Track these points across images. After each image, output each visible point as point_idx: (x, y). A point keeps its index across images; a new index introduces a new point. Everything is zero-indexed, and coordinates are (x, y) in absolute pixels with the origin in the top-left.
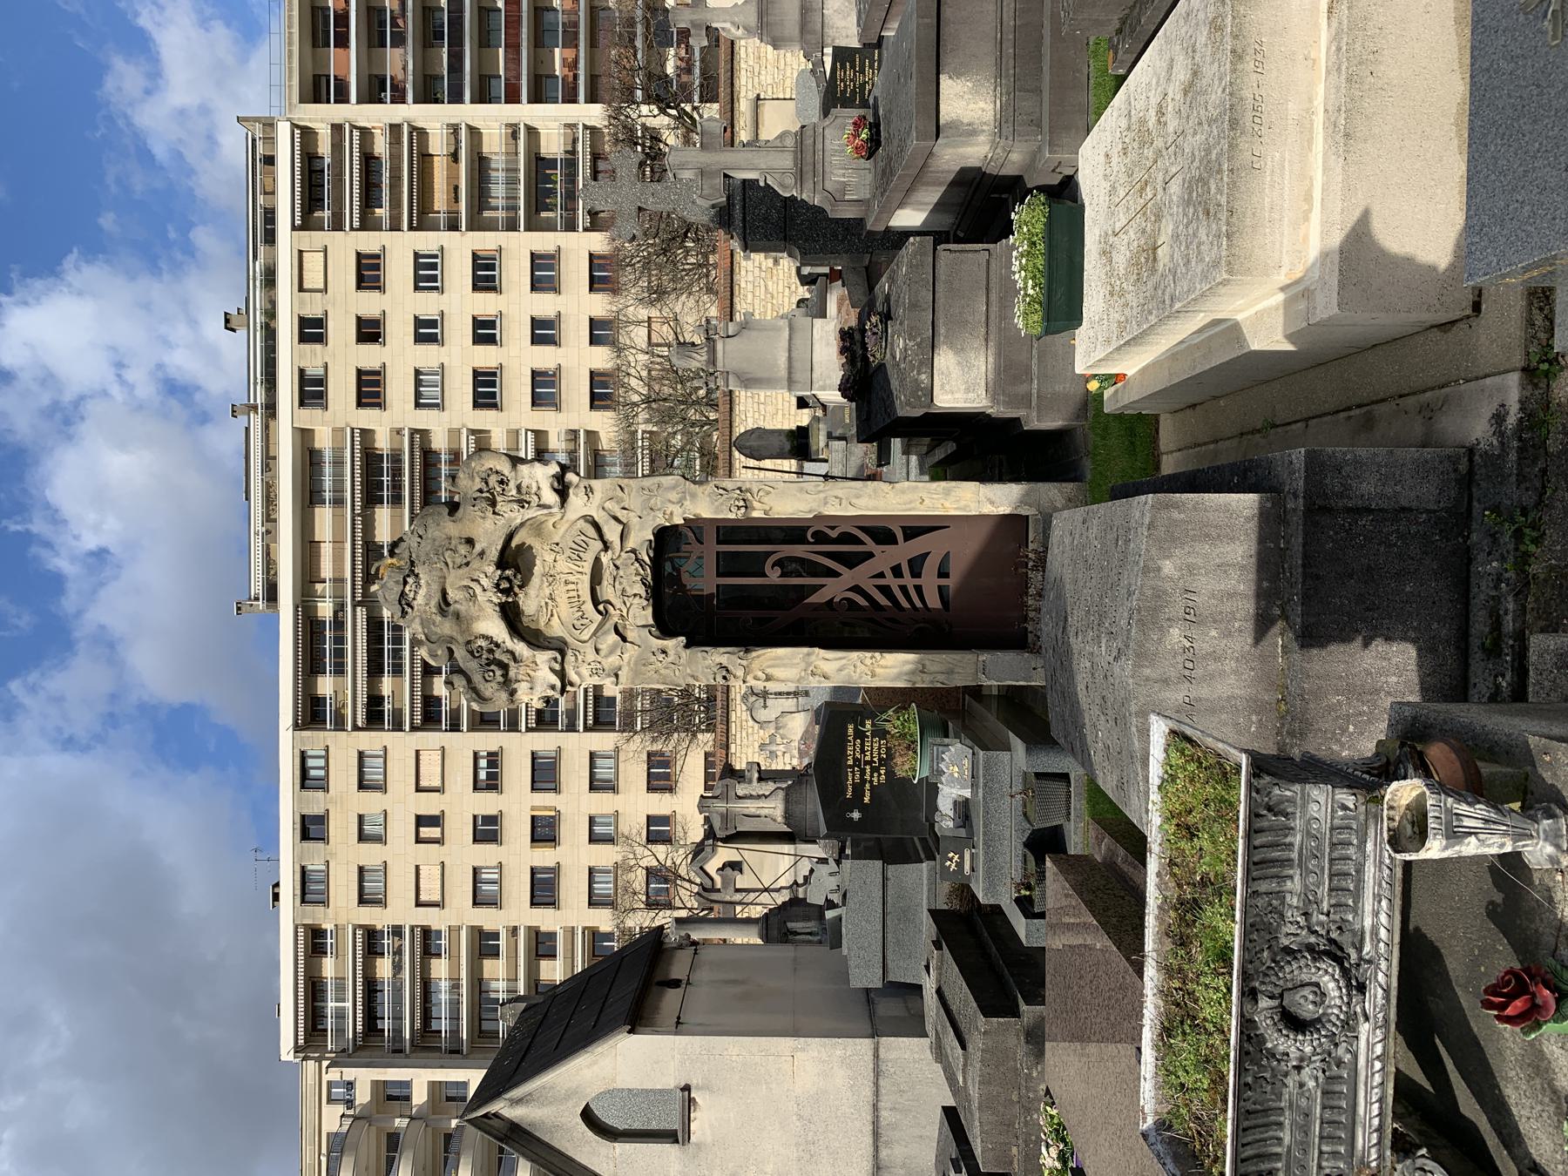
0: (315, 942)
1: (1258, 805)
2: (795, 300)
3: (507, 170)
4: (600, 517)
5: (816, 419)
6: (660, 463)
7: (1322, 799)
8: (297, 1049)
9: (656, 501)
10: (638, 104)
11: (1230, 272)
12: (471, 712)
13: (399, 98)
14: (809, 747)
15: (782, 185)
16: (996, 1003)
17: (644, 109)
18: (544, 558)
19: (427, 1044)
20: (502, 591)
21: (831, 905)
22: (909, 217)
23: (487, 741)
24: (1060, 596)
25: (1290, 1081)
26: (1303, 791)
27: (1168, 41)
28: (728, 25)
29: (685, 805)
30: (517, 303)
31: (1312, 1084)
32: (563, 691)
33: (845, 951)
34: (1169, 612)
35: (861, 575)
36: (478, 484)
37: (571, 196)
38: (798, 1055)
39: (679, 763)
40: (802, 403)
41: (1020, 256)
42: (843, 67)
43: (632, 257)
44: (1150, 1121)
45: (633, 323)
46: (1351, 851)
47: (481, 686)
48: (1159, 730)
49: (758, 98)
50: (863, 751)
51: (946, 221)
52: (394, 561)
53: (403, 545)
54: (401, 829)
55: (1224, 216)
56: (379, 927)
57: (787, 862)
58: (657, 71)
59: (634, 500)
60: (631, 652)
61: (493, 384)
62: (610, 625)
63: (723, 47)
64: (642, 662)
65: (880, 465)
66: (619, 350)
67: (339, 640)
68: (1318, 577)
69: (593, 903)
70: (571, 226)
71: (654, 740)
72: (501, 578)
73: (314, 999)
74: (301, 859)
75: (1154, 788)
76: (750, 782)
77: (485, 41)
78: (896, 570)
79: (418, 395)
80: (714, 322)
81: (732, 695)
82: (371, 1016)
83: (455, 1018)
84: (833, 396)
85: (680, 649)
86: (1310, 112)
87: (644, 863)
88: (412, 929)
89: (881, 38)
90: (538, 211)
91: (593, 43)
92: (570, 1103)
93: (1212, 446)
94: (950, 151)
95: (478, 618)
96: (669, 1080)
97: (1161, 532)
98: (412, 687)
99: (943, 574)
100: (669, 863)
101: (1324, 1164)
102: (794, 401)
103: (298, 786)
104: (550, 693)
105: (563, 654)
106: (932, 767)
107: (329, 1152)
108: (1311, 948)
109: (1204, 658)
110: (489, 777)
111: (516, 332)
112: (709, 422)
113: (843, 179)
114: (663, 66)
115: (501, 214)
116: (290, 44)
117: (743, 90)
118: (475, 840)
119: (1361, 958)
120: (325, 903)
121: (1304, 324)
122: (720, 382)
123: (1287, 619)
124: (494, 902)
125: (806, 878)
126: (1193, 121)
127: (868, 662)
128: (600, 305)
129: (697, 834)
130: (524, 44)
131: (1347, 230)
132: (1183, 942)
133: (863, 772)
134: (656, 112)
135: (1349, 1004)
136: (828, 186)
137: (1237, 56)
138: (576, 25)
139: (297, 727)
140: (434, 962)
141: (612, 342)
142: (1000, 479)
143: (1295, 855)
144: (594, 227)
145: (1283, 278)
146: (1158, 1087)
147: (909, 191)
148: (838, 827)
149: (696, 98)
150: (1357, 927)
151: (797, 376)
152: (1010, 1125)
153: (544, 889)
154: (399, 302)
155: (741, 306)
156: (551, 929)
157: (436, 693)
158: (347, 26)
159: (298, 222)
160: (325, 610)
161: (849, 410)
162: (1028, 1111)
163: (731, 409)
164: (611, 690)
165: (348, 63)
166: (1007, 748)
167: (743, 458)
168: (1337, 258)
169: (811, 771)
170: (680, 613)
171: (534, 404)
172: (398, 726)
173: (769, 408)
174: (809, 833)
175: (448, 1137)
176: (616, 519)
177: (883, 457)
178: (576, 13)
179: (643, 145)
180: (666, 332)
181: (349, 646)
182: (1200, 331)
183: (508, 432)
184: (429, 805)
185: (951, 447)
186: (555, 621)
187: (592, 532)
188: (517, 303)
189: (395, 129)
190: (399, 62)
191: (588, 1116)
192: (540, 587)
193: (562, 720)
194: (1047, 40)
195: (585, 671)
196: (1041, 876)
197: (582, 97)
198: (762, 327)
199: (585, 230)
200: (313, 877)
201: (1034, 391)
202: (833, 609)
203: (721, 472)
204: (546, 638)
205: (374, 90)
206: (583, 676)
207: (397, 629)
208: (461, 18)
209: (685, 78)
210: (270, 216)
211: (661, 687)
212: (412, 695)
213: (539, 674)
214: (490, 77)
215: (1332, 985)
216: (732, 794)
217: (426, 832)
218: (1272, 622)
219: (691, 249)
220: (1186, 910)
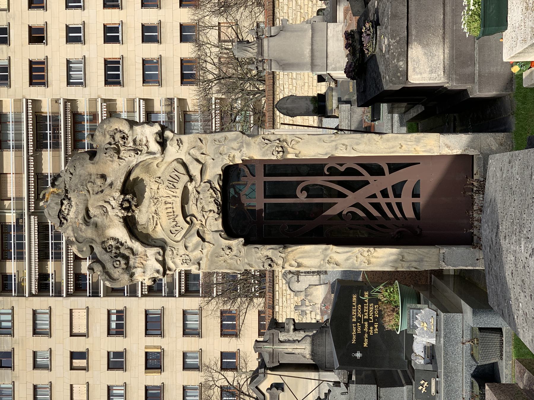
2: (316, 9)
4: (187, 159)
5: (330, 89)
9: (224, 149)
12: (106, 288)
14: (327, 308)
18: (151, 187)
20: (124, 209)
23: (116, 303)
24: (494, 212)
29: (246, 344)
32: (164, 274)
35: (360, 196)
36: (108, 139)
39: (242, 318)
40: (321, 79)
45: (208, 27)
47: (112, 271)
50: (363, 312)
52: (55, 189)
53: (60, 179)
54: (61, 361)
57: (313, 384)
61: (117, 69)
62: (194, 230)
64: (215, 255)
65: (373, 120)
66: (200, 45)
67: (20, 237)
71: (225, 303)
72: (124, 200)
76: (288, 331)
78: (384, 194)
79: (69, 77)
80: (262, 25)
84: (340, 75)
85: (241, 246)
87: (219, 384)
95: (109, 227)
98: (67, 268)
99: (415, 195)
100: (235, 384)
102: (316, 77)
104: (156, 275)
106: (409, 323)
110: (118, 327)
118: (109, 368)
122: (266, 66)
125: (326, 395)
127: (366, 254)
129: (253, 365)
133: (363, 326)
142: (454, 131)
148: (346, 362)
151: (318, 61)
155: (280, 15)
157: (83, 271)
161: (352, 85)
163: (274, 83)
164: (194, 270)
166: (460, 311)
167: (282, 115)
169: (328, 324)
170: (240, 223)
171: (144, 82)
172: (58, 294)
174: (328, 365)
176: (198, 161)
177: (376, 115)
180: (230, 33)
181: (26, 242)
183: (128, 100)
184: (79, 345)
186: (159, 228)
187: (182, 169)
193: (165, 289)
198: (294, 29)
201: (477, 72)
202: (342, 219)
203: (267, 125)
204: (153, 239)
211: (229, 271)
212: (67, 273)
213: (149, 263)
216: (276, 339)
217: (77, 363)
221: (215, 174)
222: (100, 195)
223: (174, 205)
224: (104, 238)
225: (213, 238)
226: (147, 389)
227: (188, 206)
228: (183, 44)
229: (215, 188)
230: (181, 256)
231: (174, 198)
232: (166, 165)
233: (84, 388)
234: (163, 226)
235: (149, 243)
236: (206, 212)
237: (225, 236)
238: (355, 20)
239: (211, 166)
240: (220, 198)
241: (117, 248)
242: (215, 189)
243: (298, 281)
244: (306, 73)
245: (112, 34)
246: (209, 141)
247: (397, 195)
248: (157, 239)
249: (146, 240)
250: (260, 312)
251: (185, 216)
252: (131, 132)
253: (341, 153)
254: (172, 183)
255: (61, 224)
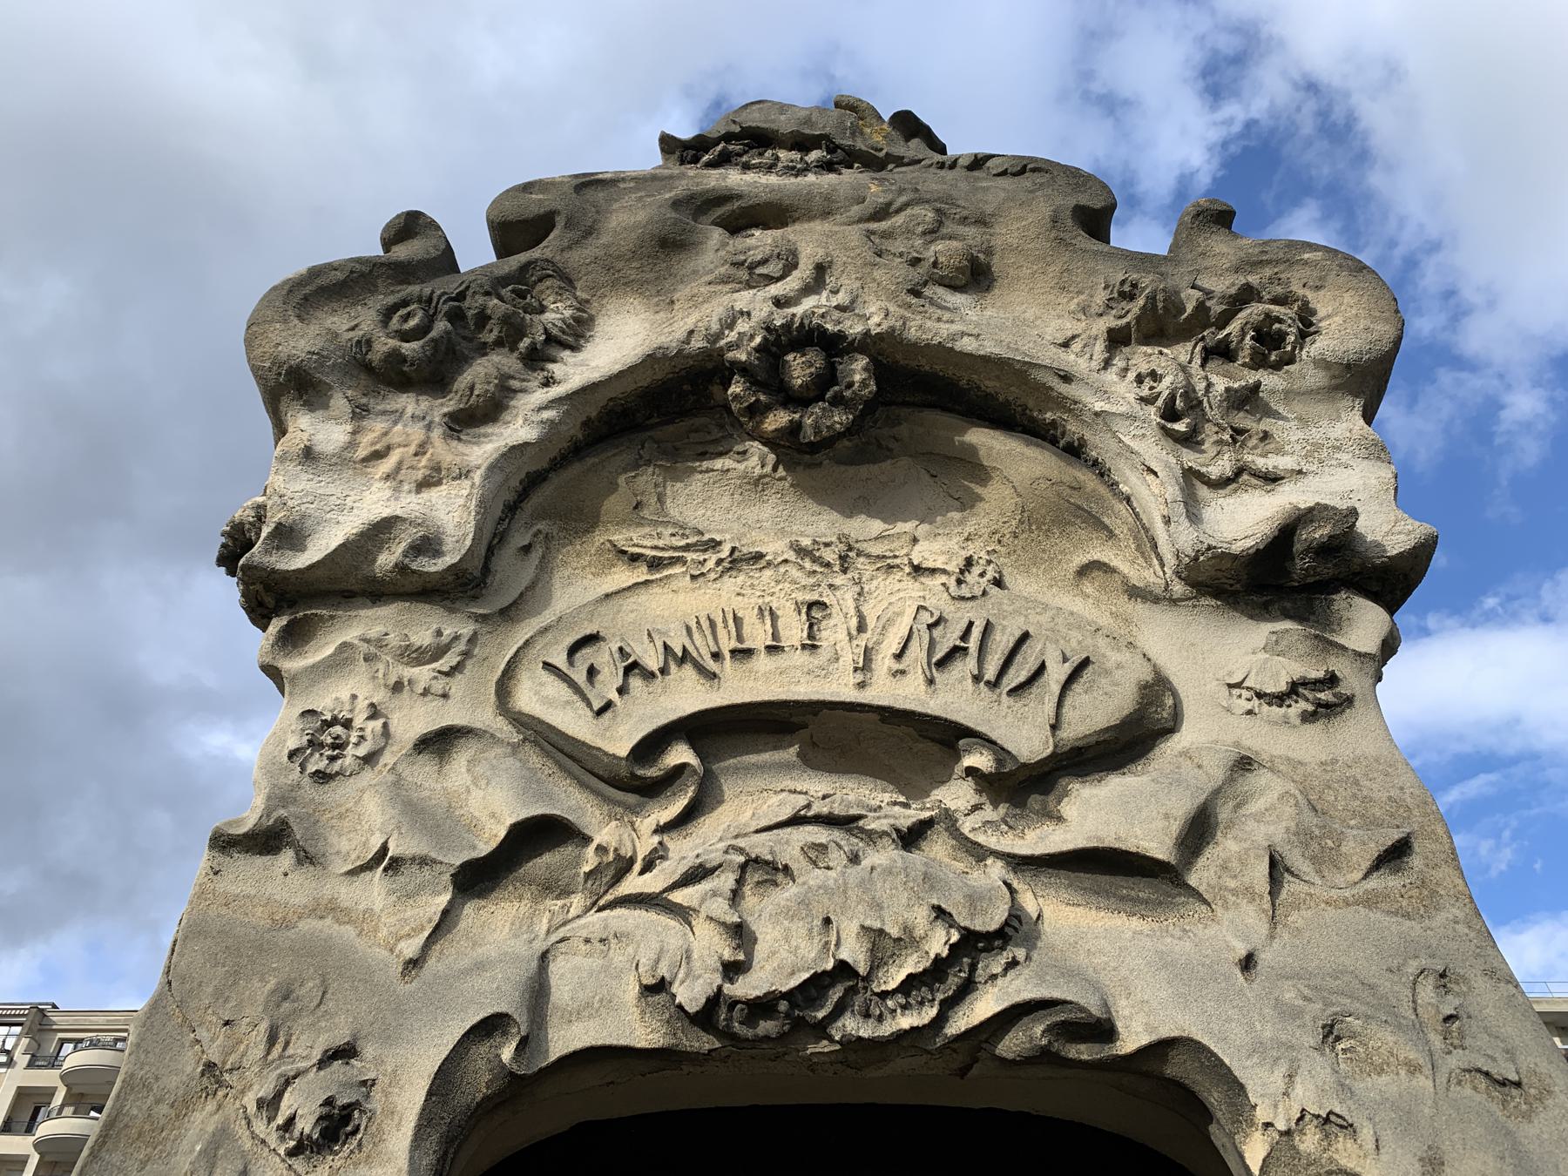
62: (570, 800)
176: (1199, 831)
187: (1094, 711)
221: (1105, 979)
223: (801, 658)
224: (593, 288)
225: (480, 966)
227: (786, 767)
229: (967, 989)
230: (374, 712)
231: (850, 655)
232: (1105, 620)
234: (631, 602)
235: (522, 516)
236: (735, 896)
237: (478, 1081)
239: (1182, 948)
240: (866, 1030)
242: (953, 982)
246: (1413, 928)
248: (545, 567)
249: (547, 498)
252: (1317, 379)
254: (973, 643)
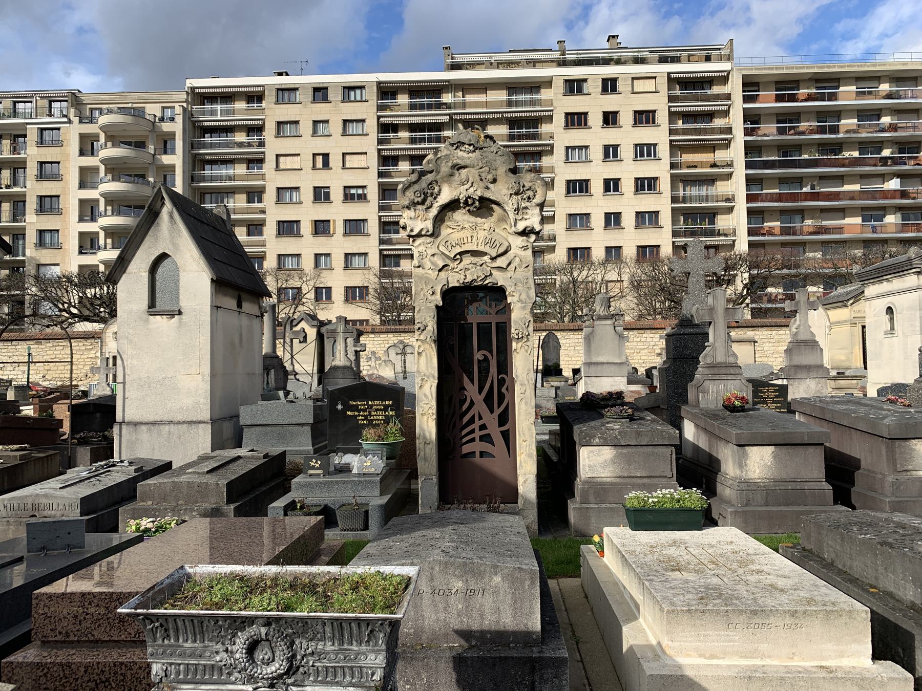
0: (255, 97)
1: (374, 625)
2: (636, 366)
3: (707, 196)
4: (510, 255)
5: (567, 380)
6: (541, 289)
7: (377, 661)
8: (193, 89)
9: (520, 287)
10: (749, 272)
11: (668, 612)
13: (747, 132)
15: (705, 357)
16: (235, 490)
17: (746, 275)
18: (486, 223)
19: (197, 162)
20: (466, 201)
21: (287, 393)
22: (689, 431)
23: (373, 193)
24: (475, 520)
25: (219, 646)
26: (382, 650)
27: (800, 575)
28: (798, 323)
30: (629, 204)
31: (218, 658)
32: (410, 236)
33: (260, 403)
34: (472, 581)
35: (480, 407)
36: (527, 185)
37: (693, 233)
38: (200, 377)
39: (363, 305)
40: (576, 372)
41: (669, 493)
42: (776, 391)
43: (659, 270)
44: (191, 571)
46: (348, 679)
47: (412, 190)
48: (410, 571)
49: (755, 342)
50: (377, 410)
51: (688, 452)
52: (483, 138)
54: (321, 145)
55: (701, 608)
56: (264, 133)
58: (770, 281)
59: (521, 274)
60: (433, 274)
61: (581, 191)
62: (448, 262)
63: (784, 320)
64: (427, 281)
65: (542, 417)
66: (603, 264)
67: (430, 107)
68: (494, 665)
69: (280, 256)
70: (675, 234)
71: (376, 290)
72: (474, 199)
73: (222, 97)
74: (303, 88)
75: (377, 568)
76: (355, 346)
77: (783, 181)
78: (483, 427)
79: (573, 148)
81: (403, 335)
82: (213, 130)
83: (212, 178)
84: (581, 389)
86: (763, 657)
88: (263, 153)
89: (794, 412)
90: (683, 214)
91: (784, 244)
92: (171, 246)
93: (563, 608)
94: (730, 454)
95: (450, 187)
96: (185, 303)
97: (517, 575)
99: (482, 454)
100: (304, 300)
101: (173, 667)
102: (577, 367)
103: (345, 85)
104: (409, 229)
105: (431, 236)
107: (134, 108)
108: (294, 656)
109: (446, 601)
110: (352, 195)
111: (612, 204)
112: (562, 317)
113: (712, 392)
114: (772, 285)
115: (681, 193)
116: (777, 68)
117: (760, 333)
118: (315, 188)
119: (288, 685)
120: (277, 103)
121: (639, 656)
122: (587, 323)
123: (469, 649)
124: (279, 200)
126: (755, 590)
127: (430, 411)
128: (629, 252)
129: (322, 316)
130: (782, 204)
131: (695, 679)
132: (292, 587)
133: (364, 410)
134: (745, 282)
135: (263, 678)
136: (707, 383)
137: (794, 614)
138: (794, 234)
139: (379, 83)
140: (244, 166)
141: (607, 260)
143: (346, 646)
144: (675, 247)
145: (665, 643)
146: (209, 574)
147: (705, 430)
149: (754, 306)
150: (306, 683)
151: (593, 368)
152: (165, 500)
153: (288, 228)
154: (627, 136)
156: (264, 233)
158: (788, 101)
159: (672, 76)
160: (447, 98)
162: (173, 510)
165: (767, 102)
168: (679, 673)
169: (362, 381)
170: (455, 301)
171: (570, 215)
172: (380, 141)
173: (572, 352)
175: (143, 176)
176: (509, 264)
177: (547, 419)
178: (801, 234)
179: (725, 275)
182: (632, 598)
185: (555, 458)
186: (450, 231)
187: (501, 250)
188: (629, 204)
189: (729, 130)
190: (768, 131)
191: (163, 256)
192: (469, 222)
194: (797, 509)
195: (421, 248)
196: (309, 514)
197: (752, 238)
199: (673, 243)
200: (292, 95)
204: (440, 226)
205: (752, 118)
206: (418, 247)
207: (438, 140)
208: (796, 167)
209: (765, 298)
210: (676, 60)
214: (762, 185)
215: (274, 669)
216: (348, 335)
217: (319, 159)
218: (467, 640)
219: (664, 304)
220: (310, 587)
222: (478, 179)
226: (298, 222)
228: (604, 249)
233: (297, 166)
238: (632, 400)
241: (432, 194)
243: (397, 354)
244: (583, 359)
245: (612, 185)
247: (482, 438)
250: (367, 321)
251: (461, 254)
253: (518, 388)
255: (452, 145)
